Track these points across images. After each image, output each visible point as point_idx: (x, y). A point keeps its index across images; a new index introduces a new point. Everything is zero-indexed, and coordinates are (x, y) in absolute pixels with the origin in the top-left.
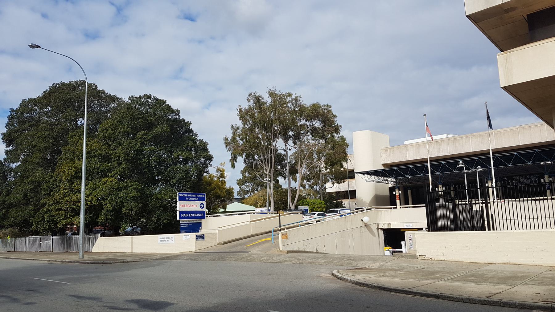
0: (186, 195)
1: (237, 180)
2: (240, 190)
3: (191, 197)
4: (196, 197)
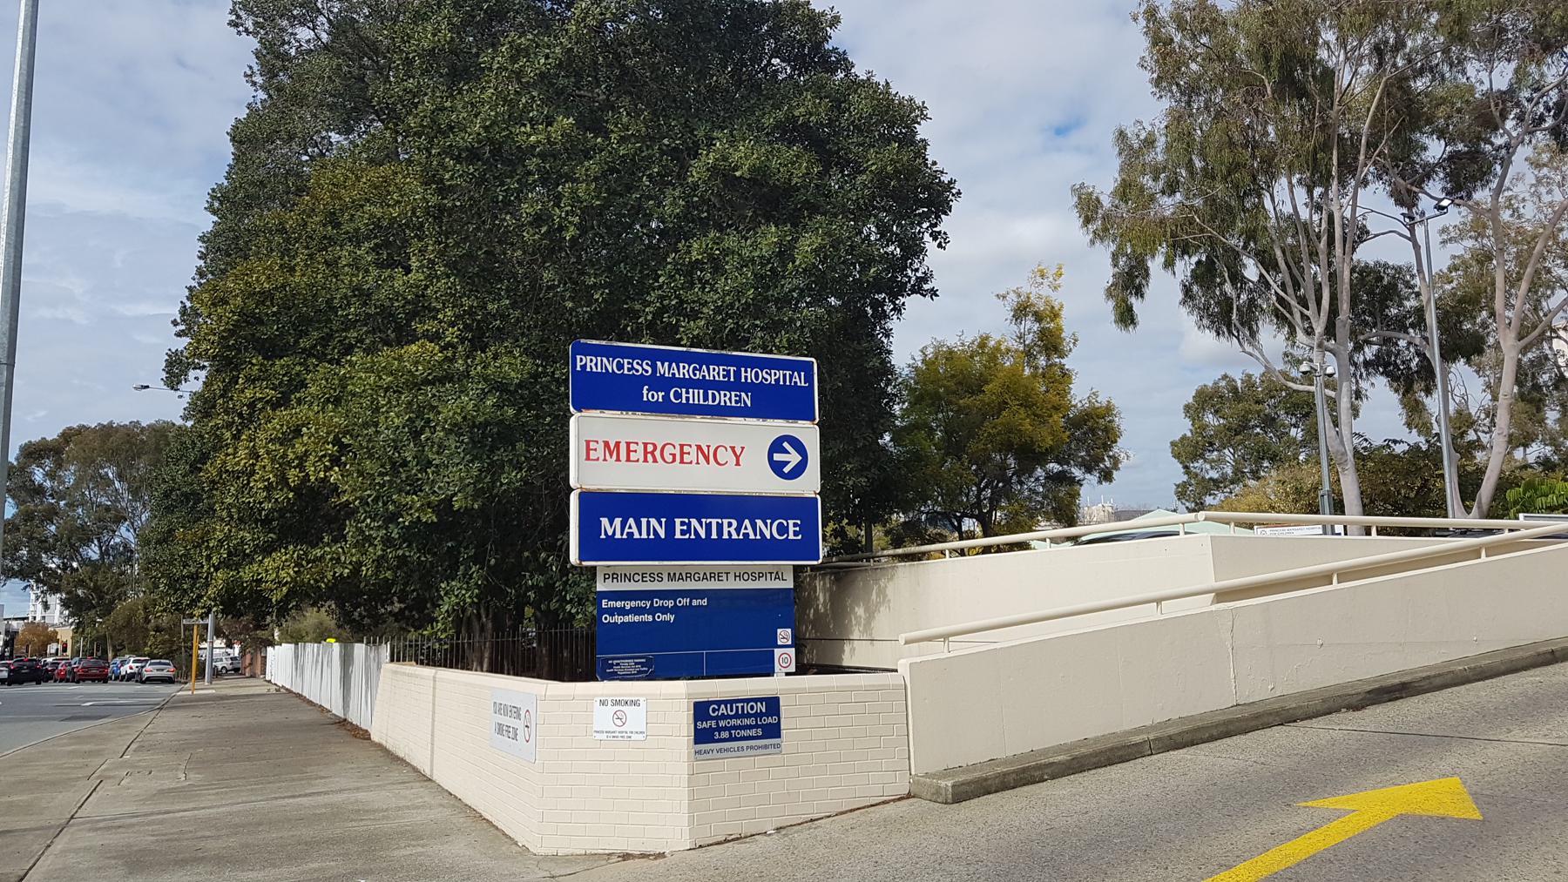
0: (643, 368)
1: (1173, 444)
2: (1185, 478)
3: (689, 384)
4: (737, 386)
